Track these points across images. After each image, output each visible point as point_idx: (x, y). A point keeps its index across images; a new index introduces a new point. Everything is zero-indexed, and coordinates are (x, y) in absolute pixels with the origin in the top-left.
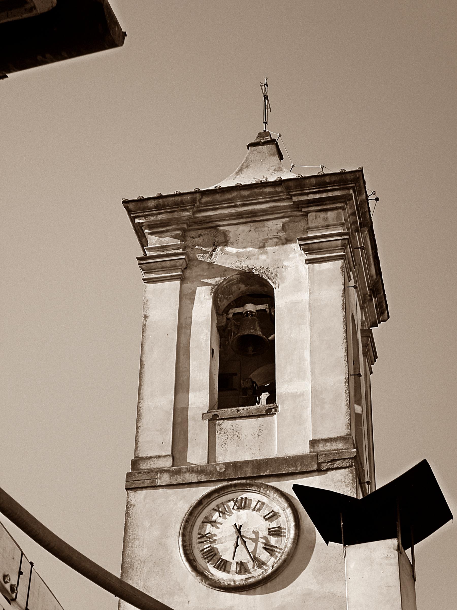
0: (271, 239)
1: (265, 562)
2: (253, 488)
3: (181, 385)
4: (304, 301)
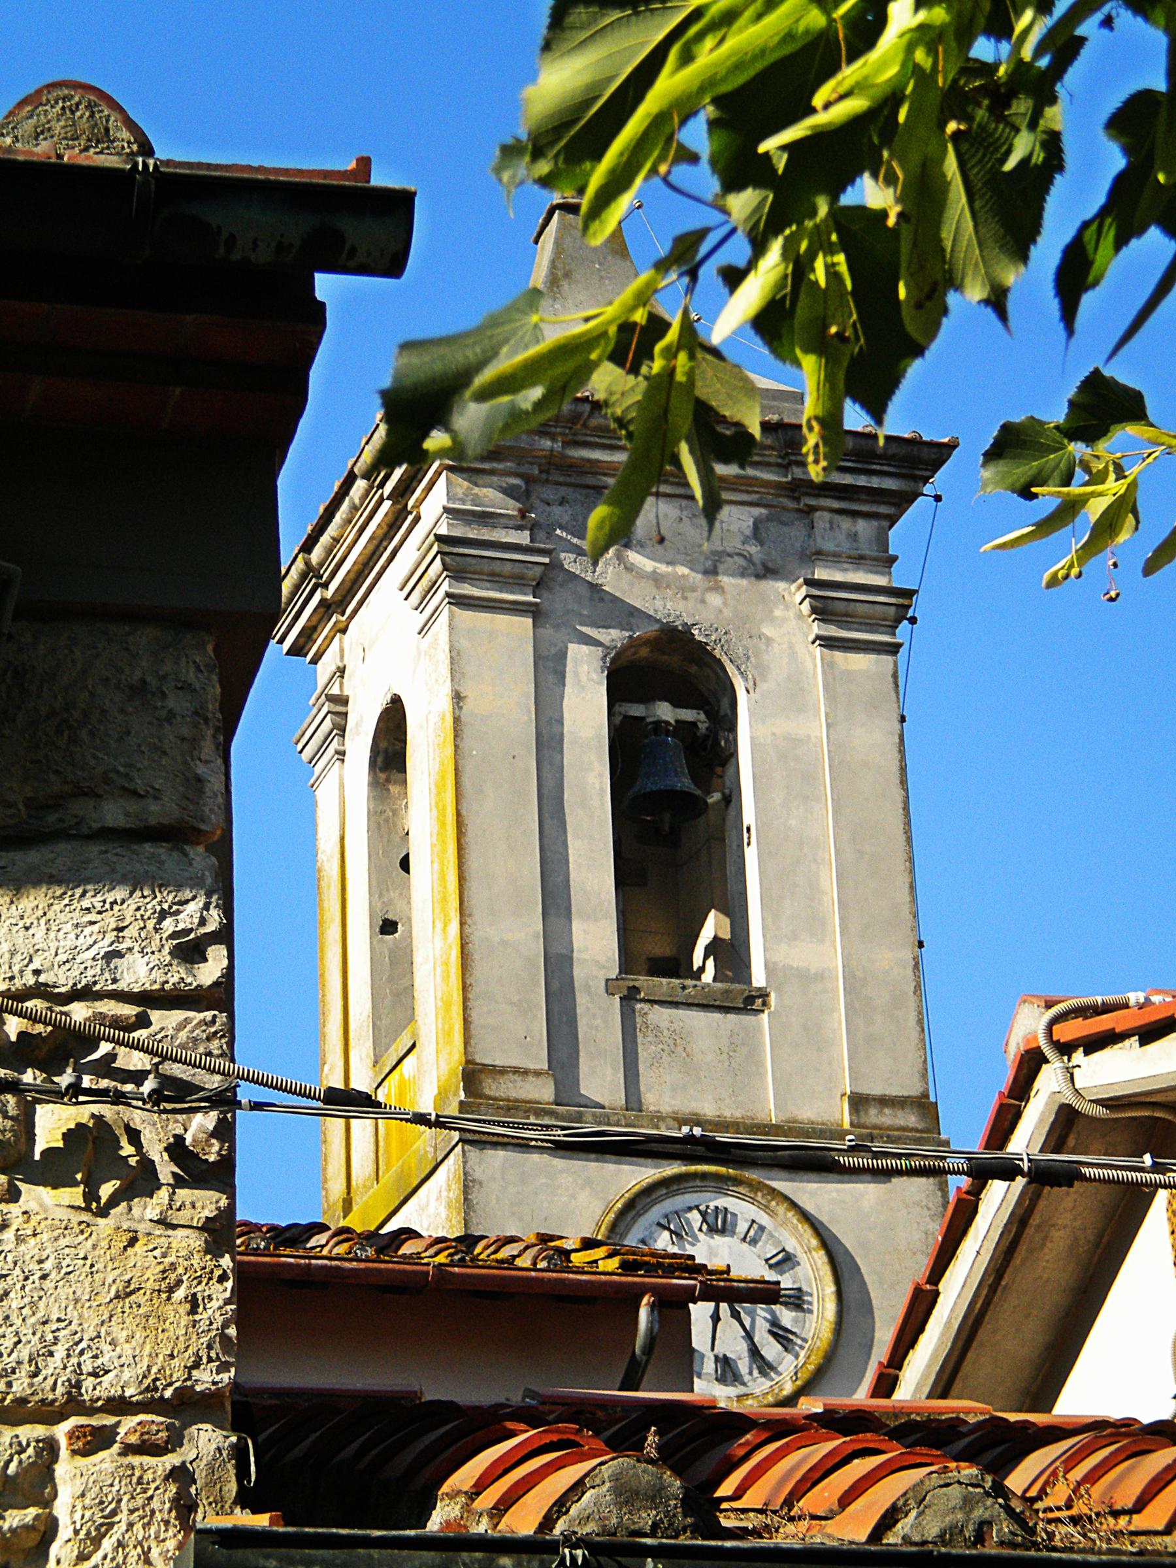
0: (729, 555)
1: (775, 1364)
2: (741, 1189)
3: (555, 898)
4: (813, 740)
